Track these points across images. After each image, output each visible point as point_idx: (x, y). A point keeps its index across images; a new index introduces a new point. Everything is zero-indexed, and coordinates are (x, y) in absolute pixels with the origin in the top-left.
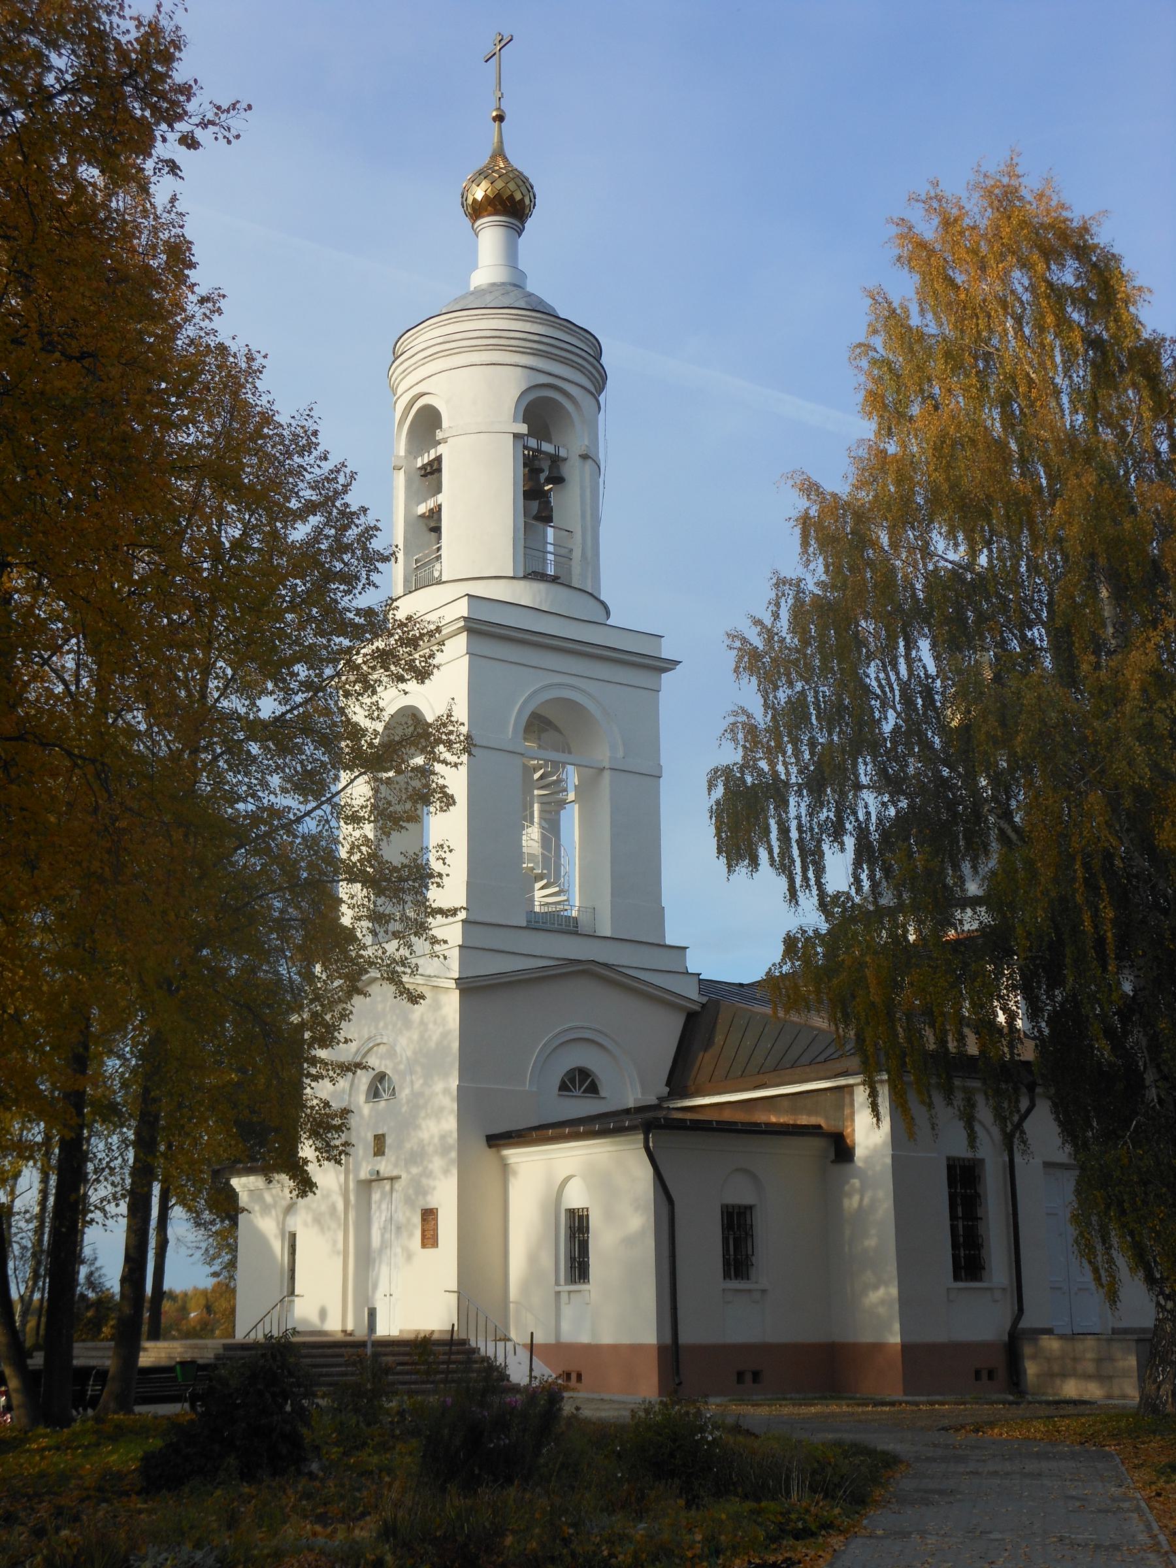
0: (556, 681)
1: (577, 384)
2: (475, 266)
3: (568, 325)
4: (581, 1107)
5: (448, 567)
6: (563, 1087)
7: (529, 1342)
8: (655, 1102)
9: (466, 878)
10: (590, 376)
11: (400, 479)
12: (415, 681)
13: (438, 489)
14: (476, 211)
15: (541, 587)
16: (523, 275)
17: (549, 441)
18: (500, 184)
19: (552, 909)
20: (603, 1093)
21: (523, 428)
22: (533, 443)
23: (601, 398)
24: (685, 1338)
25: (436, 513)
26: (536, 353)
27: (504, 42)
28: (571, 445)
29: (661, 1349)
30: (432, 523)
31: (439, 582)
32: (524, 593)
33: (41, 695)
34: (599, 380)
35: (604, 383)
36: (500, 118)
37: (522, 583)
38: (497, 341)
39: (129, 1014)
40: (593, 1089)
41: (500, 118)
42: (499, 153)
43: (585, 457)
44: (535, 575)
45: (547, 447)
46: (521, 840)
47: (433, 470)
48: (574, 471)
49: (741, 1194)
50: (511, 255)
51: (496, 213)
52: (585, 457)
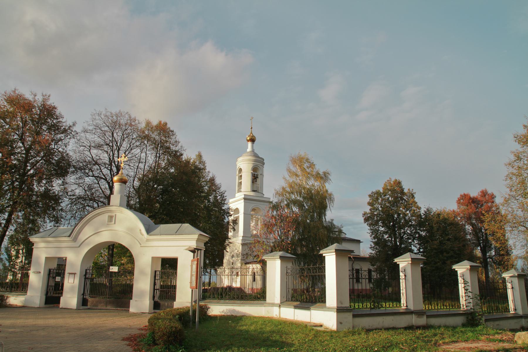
1: (138, 240)
2: (248, 148)
5: (242, 190)
11: (237, 177)
13: (241, 179)
14: (248, 141)
15: (254, 193)
16: (254, 150)
17: (256, 172)
21: (252, 172)
22: (254, 173)
23: (264, 166)
25: (241, 182)
26: (254, 161)
27: (252, 118)
28: (259, 173)
30: (241, 183)
31: (241, 192)
32: (252, 194)
33: (41, 124)
34: (264, 164)
36: (252, 128)
38: (249, 160)
39: (211, 331)
41: (252, 128)
42: (252, 133)
43: (261, 174)
44: (254, 191)
45: (256, 173)
46: (488, 274)
47: (241, 176)
48: (259, 176)
50: (252, 147)
52: (261, 174)
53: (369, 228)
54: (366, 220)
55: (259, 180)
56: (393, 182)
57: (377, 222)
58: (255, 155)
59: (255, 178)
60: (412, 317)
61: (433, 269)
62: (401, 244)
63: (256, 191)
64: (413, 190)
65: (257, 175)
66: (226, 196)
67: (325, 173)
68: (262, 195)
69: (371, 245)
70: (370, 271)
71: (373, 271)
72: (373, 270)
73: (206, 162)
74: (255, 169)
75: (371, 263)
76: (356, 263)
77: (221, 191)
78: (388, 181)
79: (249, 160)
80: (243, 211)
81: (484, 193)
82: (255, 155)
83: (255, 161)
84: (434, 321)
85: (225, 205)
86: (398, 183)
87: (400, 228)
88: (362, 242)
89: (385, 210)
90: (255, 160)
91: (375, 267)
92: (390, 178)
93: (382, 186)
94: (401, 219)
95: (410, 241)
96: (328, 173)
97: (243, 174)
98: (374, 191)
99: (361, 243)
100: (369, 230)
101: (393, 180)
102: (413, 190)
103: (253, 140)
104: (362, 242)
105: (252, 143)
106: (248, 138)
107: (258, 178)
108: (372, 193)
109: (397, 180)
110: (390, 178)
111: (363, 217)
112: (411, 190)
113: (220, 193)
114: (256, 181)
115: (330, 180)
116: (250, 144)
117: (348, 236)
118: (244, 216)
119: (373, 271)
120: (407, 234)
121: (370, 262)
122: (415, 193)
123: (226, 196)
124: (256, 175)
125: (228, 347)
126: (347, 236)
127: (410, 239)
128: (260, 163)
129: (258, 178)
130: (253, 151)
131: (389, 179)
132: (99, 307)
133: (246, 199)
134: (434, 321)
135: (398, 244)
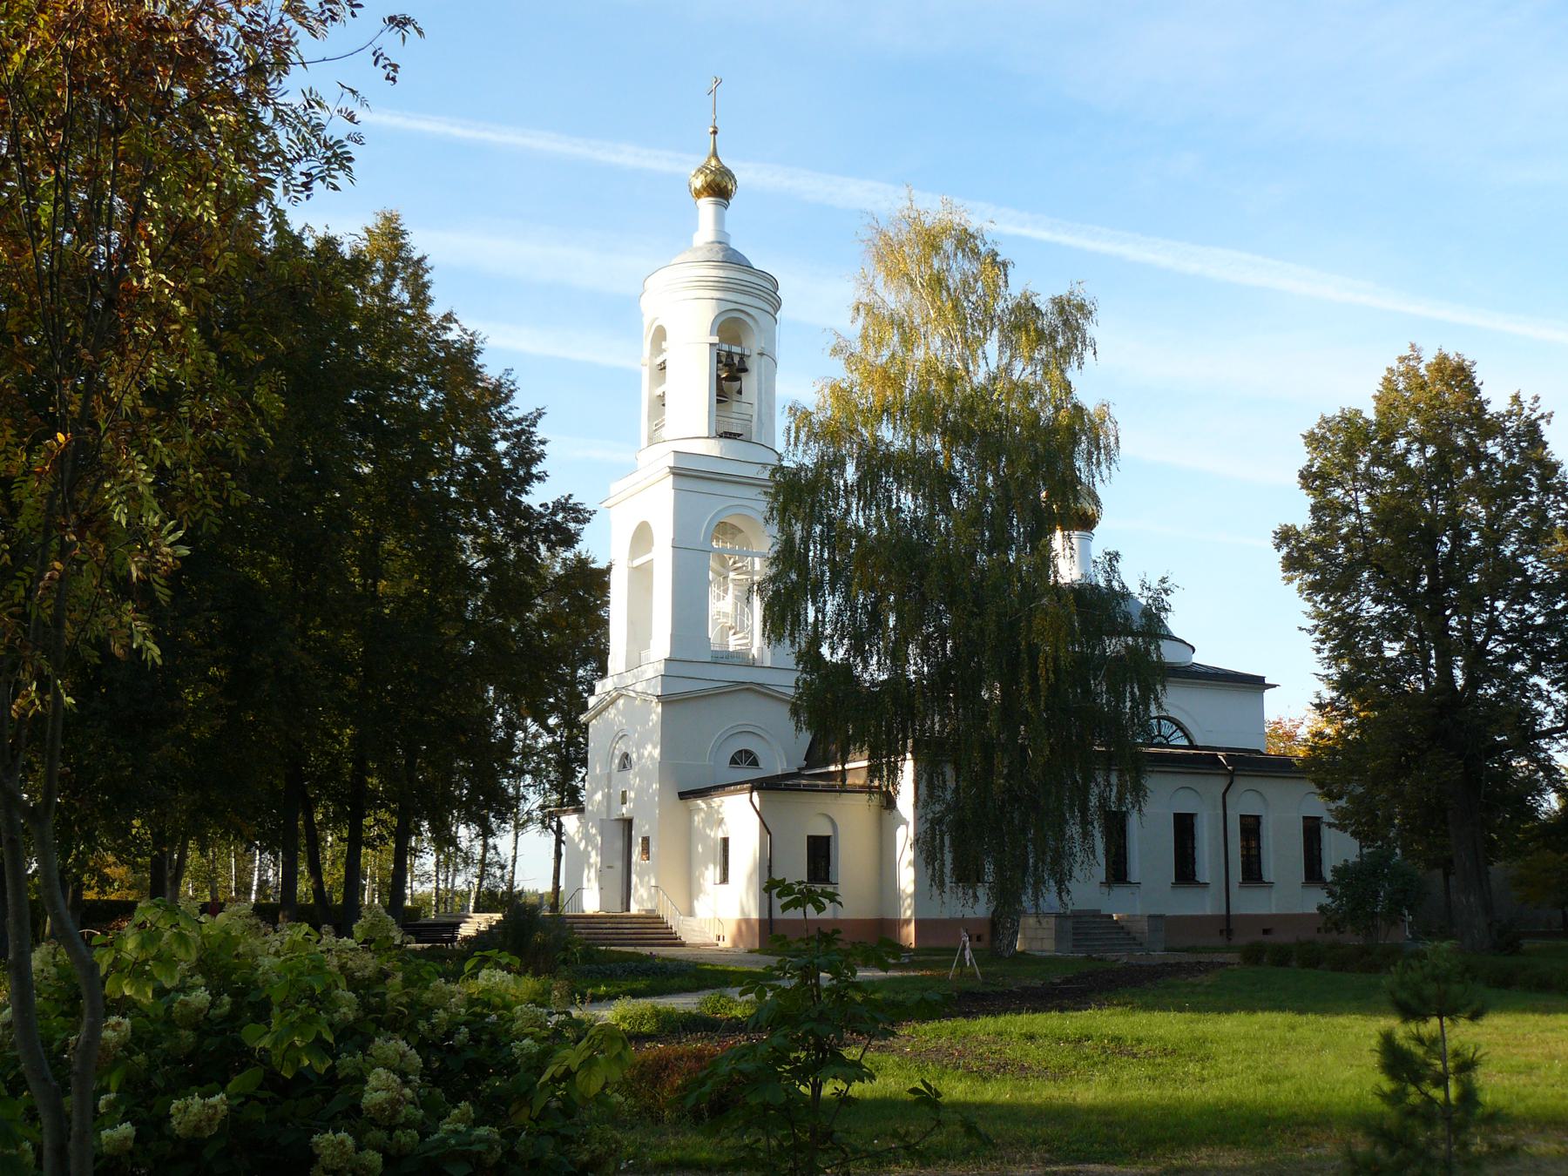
0: (736, 503)
6: (733, 761)
7: (1224, 912)
8: (796, 771)
9: (670, 632)
12: (1299, 528)
14: (698, 194)
17: (739, 344)
18: (709, 178)
19: (738, 648)
20: (761, 766)
21: (715, 339)
23: (777, 316)
24: (1232, 912)
25: (662, 397)
27: (718, 82)
28: (752, 345)
29: (761, 921)
32: (713, 448)
34: (777, 304)
35: (780, 305)
36: (715, 132)
37: (713, 441)
38: (702, 283)
41: (715, 132)
42: (715, 155)
43: (761, 354)
45: (736, 349)
48: (753, 364)
49: (823, 830)
50: (720, 221)
51: (710, 195)
52: (761, 354)
53: (1308, 607)
54: (1293, 564)
55: (750, 382)
56: (1428, 366)
57: (1352, 569)
58: (732, 259)
60: (1481, 1056)
62: (1473, 682)
63: (740, 435)
64: (1537, 399)
65: (742, 356)
66: (543, 442)
67: (1061, 305)
69: (1318, 695)
70: (1312, 828)
71: (1330, 825)
72: (1327, 818)
73: (428, 263)
74: (730, 328)
75: (1321, 785)
76: (1241, 784)
77: (517, 414)
78: (1402, 359)
79: (702, 283)
80: (670, 535)
82: (732, 259)
83: (725, 285)
84: (1092, 919)
85: (535, 483)
86: (1458, 375)
87: (1472, 601)
88: (1274, 686)
89: (1391, 517)
90: (728, 280)
91: (1343, 803)
92: (1413, 346)
93: (1375, 387)
95: (1518, 667)
96: (1081, 307)
98: (1333, 411)
99: (1268, 693)
100: (1309, 615)
101: (1429, 357)
102: (1537, 399)
103: (720, 188)
104: (1274, 686)
105: (716, 204)
106: (698, 183)
107: (745, 370)
108: (1319, 426)
109: (1445, 358)
111: (1278, 547)
112: (1526, 398)
113: (509, 424)
114: (740, 392)
116: (707, 205)
117: (1206, 656)
118: (673, 552)
119: (1330, 825)
120: (1502, 632)
121: (1313, 780)
122: (1551, 415)
123: (543, 442)
124: (736, 359)
126: (1197, 658)
127: (1520, 658)
128: (758, 297)
129: (745, 370)
131: (1407, 352)
132: (1441, 1050)
133: (686, 474)
134: (1092, 919)
135: (1460, 682)
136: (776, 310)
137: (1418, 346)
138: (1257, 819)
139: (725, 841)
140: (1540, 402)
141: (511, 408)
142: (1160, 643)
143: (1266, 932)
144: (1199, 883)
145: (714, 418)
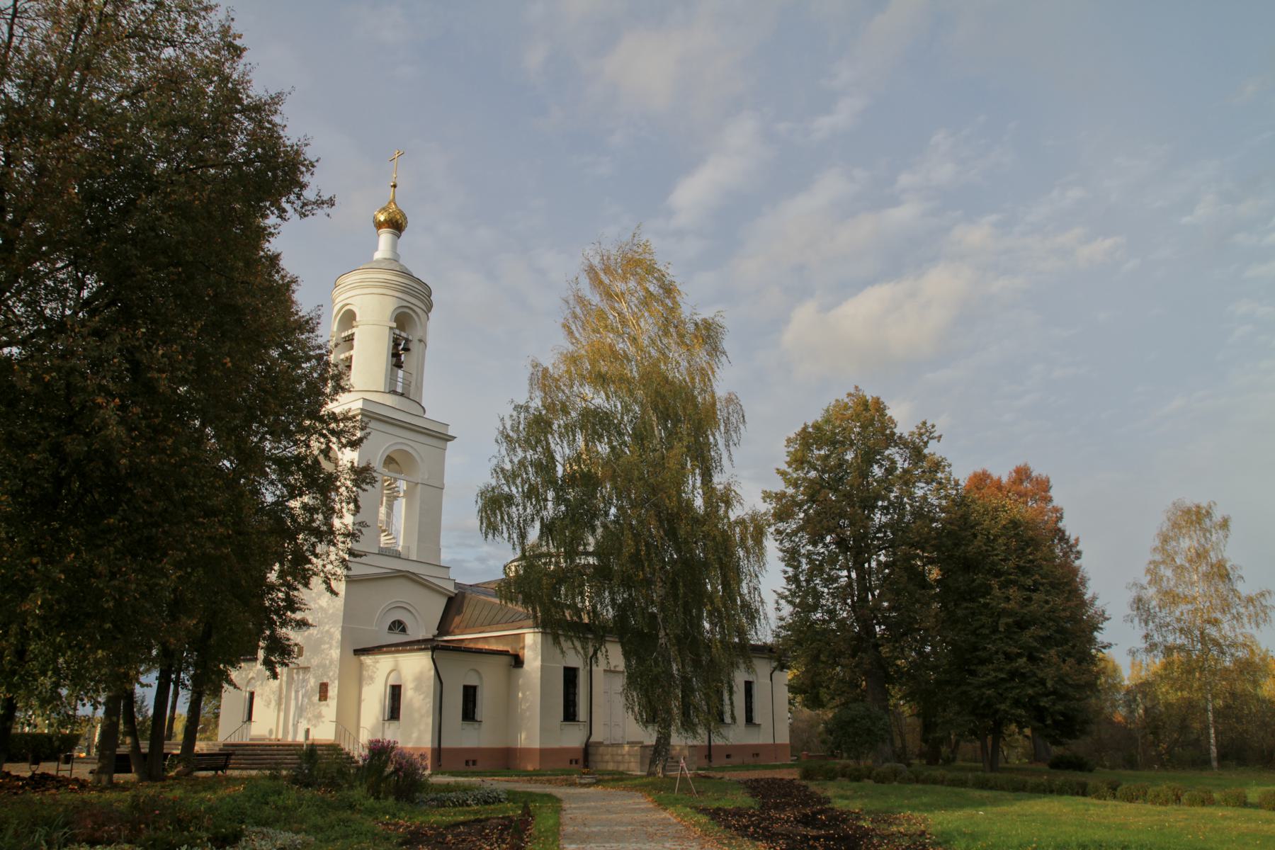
2: (376, 249)
3: (418, 281)
4: (398, 638)
7: (706, 743)
10: (425, 305)
13: (352, 348)
14: (379, 225)
17: (404, 331)
20: (408, 632)
21: (394, 325)
22: (397, 332)
29: (433, 750)
32: (390, 400)
34: (429, 307)
36: (395, 186)
37: (388, 395)
38: (386, 284)
40: (404, 630)
41: (395, 186)
42: (393, 201)
43: (420, 341)
48: (414, 346)
49: (472, 681)
50: (394, 247)
51: (389, 227)
52: (420, 341)
59: (399, 352)
61: (1003, 676)
68: (419, 411)
74: (402, 320)
81: (1022, 474)
88: (774, 591)
92: (856, 387)
94: (940, 504)
97: (360, 333)
103: (396, 225)
104: (774, 591)
110: (856, 387)
115: (724, 353)
116: (385, 237)
125: (109, 845)
130: (395, 259)
136: (430, 311)
137: (860, 387)
138: (474, 688)
139: (252, 694)
140: (935, 428)
141: (317, 336)
142: (504, 577)
143: (728, 756)
144: (755, 724)
145: (388, 380)
